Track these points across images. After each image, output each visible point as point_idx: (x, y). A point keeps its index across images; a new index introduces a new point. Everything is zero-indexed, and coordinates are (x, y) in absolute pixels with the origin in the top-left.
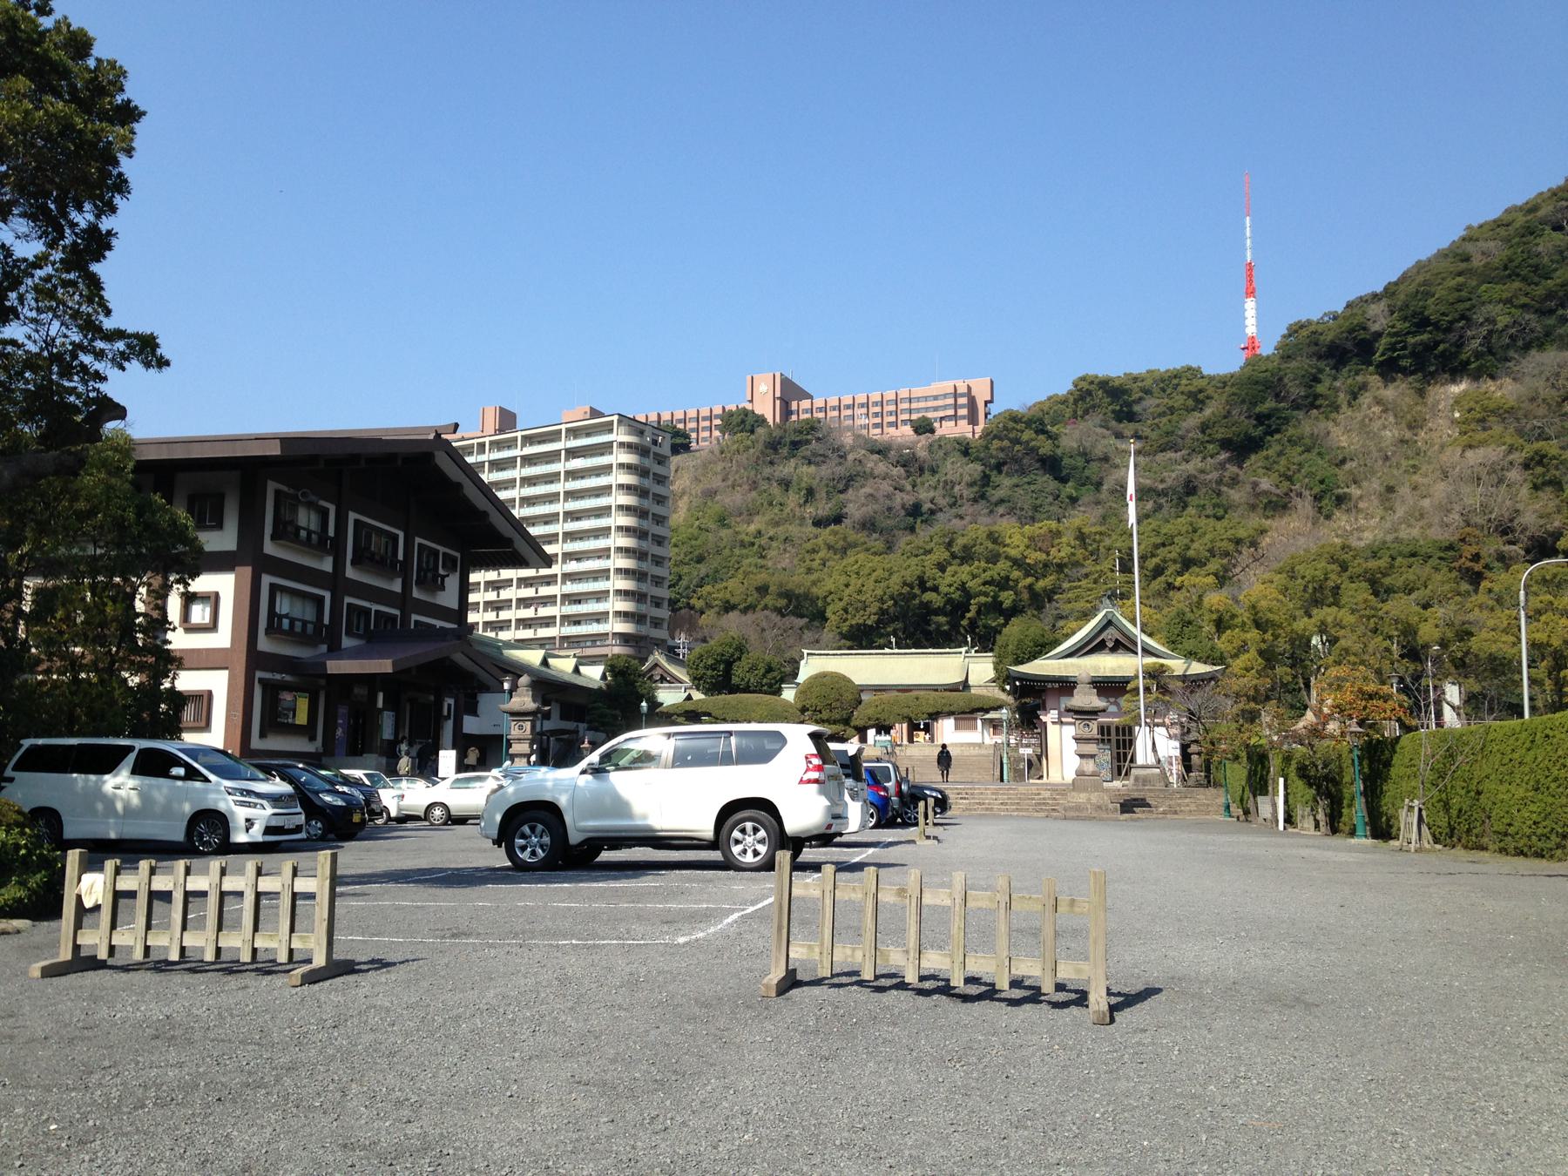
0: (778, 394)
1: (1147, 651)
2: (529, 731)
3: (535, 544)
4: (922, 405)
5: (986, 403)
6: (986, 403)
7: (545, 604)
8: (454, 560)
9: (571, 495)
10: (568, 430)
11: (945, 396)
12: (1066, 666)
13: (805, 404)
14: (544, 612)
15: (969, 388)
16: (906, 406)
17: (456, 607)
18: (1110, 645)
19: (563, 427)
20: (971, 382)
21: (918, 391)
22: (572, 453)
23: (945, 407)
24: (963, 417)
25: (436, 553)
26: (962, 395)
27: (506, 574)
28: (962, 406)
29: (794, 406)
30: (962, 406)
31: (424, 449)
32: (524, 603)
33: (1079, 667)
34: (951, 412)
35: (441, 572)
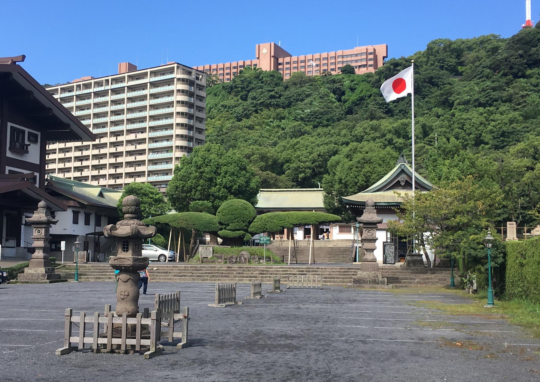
0: (273, 54)
1: (420, 186)
2: (43, 234)
3: (85, 129)
4: (349, 59)
5: (384, 58)
6: (384, 58)
7: (139, 165)
8: (36, 136)
9: (153, 107)
10: (151, 72)
11: (361, 54)
12: (376, 196)
13: (287, 59)
14: (139, 169)
15: (375, 50)
16: (340, 59)
17: (38, 162)
18: (403, 184)
19: (149, 71)
20: (377, 47)
21: (347, 52)
22: (154, 85)
23: (361, 60)
24: (371, 66)
25: (23, 132)
26: (370, 54)
27: (69, 145)
28: (370, 60)
29: (280, 60)
30: (370, 60)
31: (6, 71)
32: (129, 164)
33: (384, 197)
34: (364, 63)
35: (27, 142)
